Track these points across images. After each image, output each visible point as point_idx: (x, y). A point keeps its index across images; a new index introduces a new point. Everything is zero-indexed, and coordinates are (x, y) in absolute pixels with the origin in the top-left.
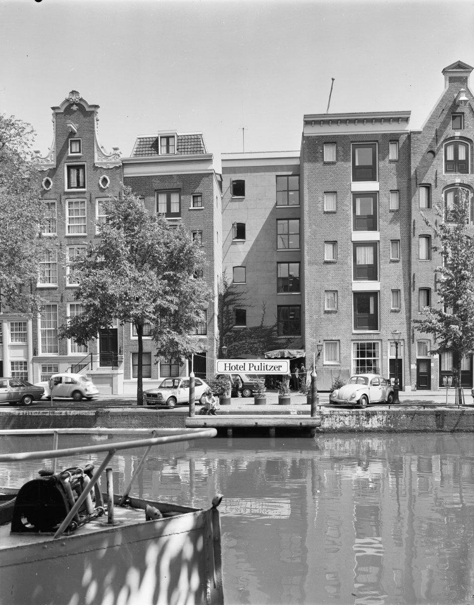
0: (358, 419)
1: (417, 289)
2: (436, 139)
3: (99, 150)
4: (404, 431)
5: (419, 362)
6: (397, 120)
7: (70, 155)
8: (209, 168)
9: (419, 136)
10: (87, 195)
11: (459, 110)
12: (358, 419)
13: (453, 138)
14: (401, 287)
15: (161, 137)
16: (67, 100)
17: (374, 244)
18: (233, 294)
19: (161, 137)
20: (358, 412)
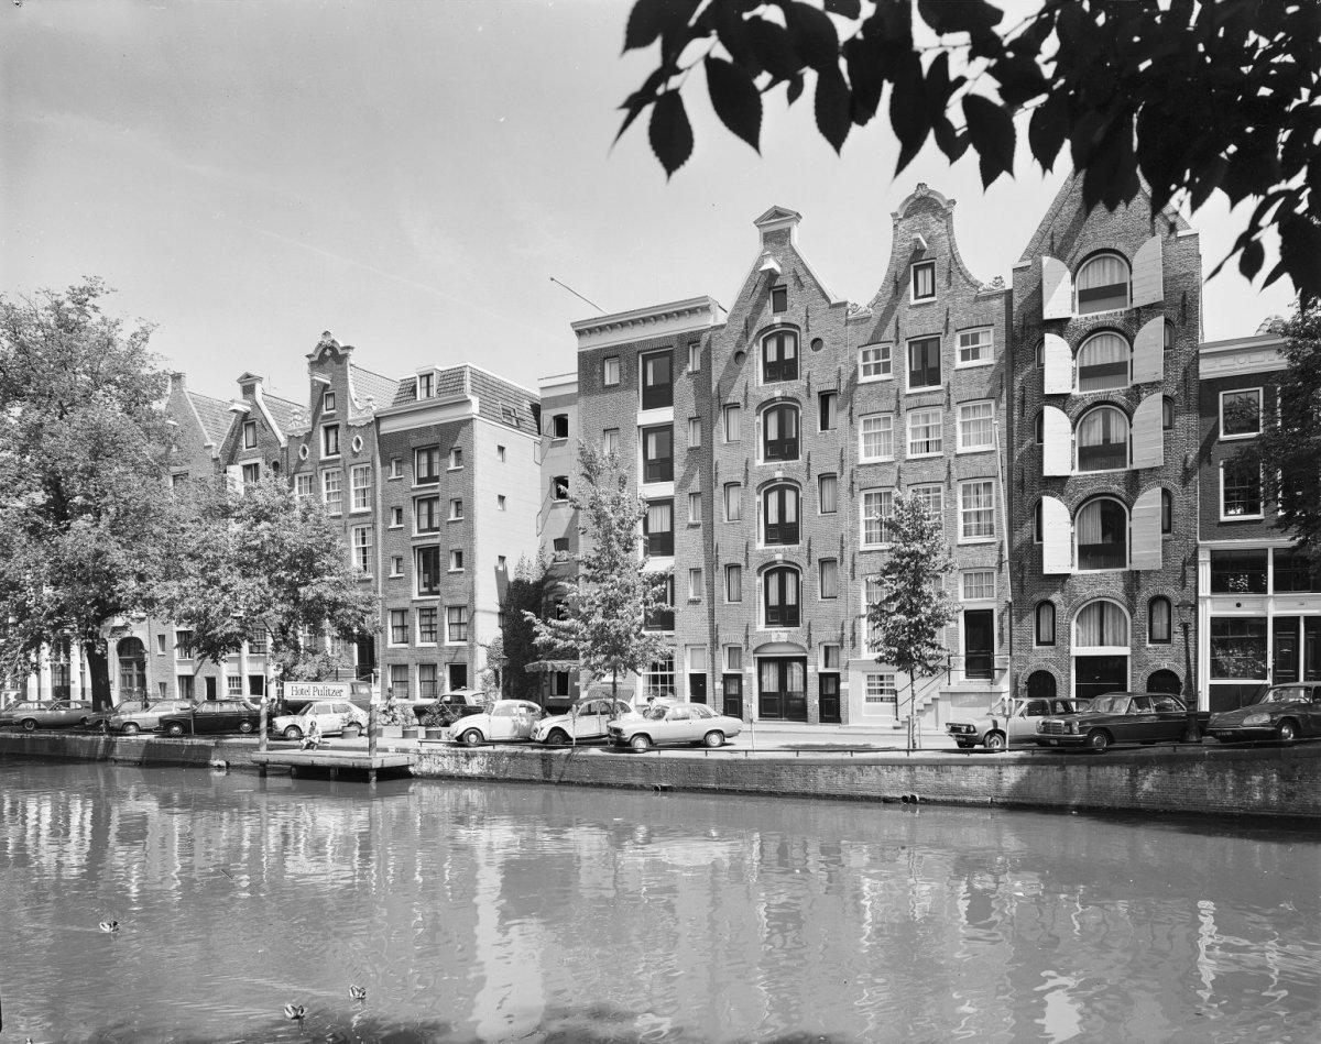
0: (458, 761)
1: (721, 567)
2: (746, 334)
3: (353, 404)
4: (510, 781)
5: (727, 678)
6: (692, 311)
7: (325, 413)
8: (469, 412)
9: (723, 332)
10: (341, 463)
11: (778, 283)
12: (458, 761)
13: (772, 327)
14: (702, 565)
15: (421, 377)
16: (913, 196)
17: (667, 502)
18: (553, 578)
19: (421, 377)
20: (456, 752)
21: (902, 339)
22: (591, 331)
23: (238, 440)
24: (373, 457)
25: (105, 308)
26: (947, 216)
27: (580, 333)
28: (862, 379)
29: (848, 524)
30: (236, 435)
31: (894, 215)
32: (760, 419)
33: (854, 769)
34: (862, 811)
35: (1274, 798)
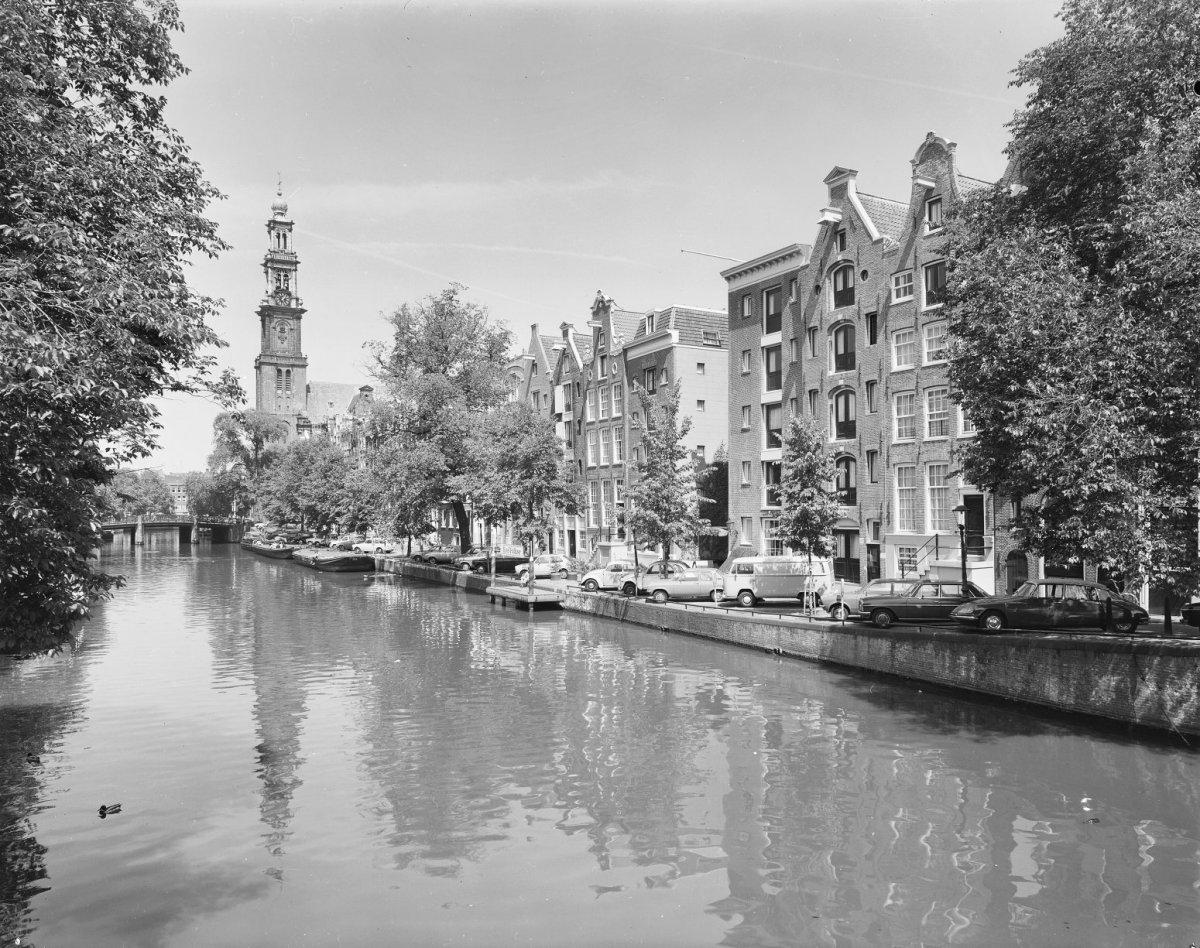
9: (807, 271)
16: (924, 144)
21: (919, 265)
22: (734, 276)
23: (561, 368)
24: (622, 380)
25: (462, 299)
26: (949, 157)
27: (728, 279)
28: (895, 301)
29: (884, 422)
30: (560, 364)
31: (913, 162)
32: (833, 338)
33: (750, 626)
34: (754, 657)
35: (972, 676)
